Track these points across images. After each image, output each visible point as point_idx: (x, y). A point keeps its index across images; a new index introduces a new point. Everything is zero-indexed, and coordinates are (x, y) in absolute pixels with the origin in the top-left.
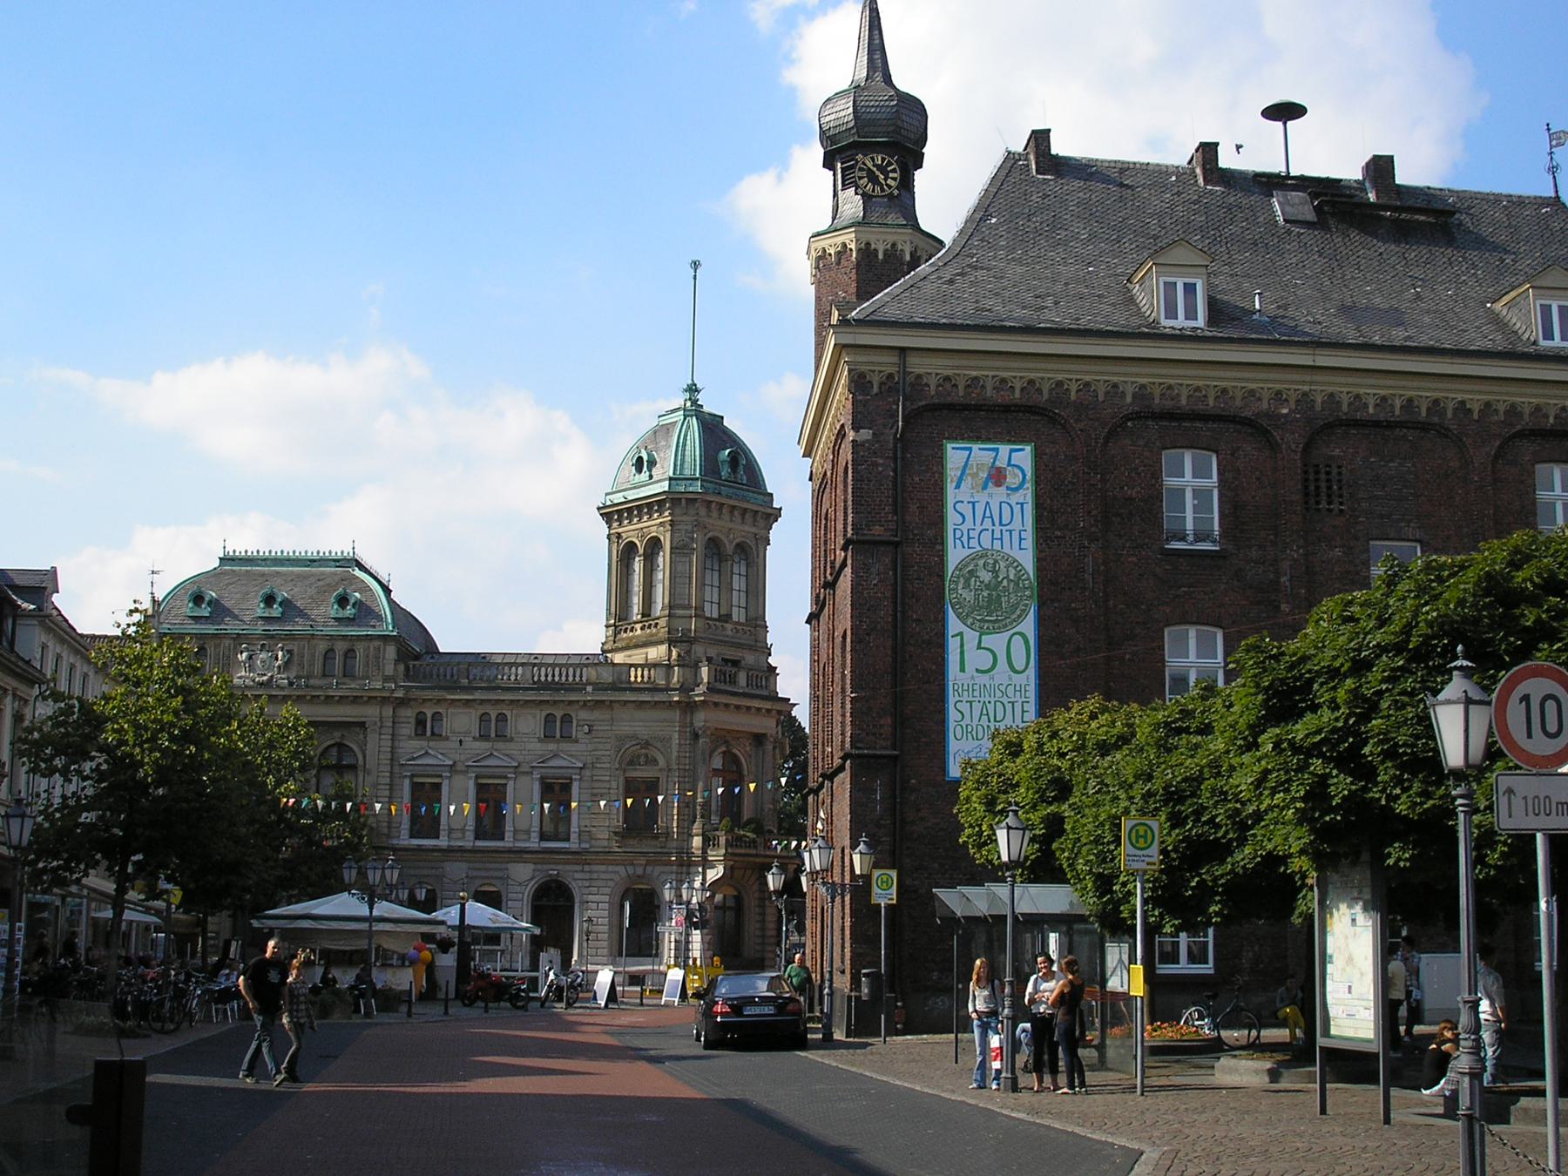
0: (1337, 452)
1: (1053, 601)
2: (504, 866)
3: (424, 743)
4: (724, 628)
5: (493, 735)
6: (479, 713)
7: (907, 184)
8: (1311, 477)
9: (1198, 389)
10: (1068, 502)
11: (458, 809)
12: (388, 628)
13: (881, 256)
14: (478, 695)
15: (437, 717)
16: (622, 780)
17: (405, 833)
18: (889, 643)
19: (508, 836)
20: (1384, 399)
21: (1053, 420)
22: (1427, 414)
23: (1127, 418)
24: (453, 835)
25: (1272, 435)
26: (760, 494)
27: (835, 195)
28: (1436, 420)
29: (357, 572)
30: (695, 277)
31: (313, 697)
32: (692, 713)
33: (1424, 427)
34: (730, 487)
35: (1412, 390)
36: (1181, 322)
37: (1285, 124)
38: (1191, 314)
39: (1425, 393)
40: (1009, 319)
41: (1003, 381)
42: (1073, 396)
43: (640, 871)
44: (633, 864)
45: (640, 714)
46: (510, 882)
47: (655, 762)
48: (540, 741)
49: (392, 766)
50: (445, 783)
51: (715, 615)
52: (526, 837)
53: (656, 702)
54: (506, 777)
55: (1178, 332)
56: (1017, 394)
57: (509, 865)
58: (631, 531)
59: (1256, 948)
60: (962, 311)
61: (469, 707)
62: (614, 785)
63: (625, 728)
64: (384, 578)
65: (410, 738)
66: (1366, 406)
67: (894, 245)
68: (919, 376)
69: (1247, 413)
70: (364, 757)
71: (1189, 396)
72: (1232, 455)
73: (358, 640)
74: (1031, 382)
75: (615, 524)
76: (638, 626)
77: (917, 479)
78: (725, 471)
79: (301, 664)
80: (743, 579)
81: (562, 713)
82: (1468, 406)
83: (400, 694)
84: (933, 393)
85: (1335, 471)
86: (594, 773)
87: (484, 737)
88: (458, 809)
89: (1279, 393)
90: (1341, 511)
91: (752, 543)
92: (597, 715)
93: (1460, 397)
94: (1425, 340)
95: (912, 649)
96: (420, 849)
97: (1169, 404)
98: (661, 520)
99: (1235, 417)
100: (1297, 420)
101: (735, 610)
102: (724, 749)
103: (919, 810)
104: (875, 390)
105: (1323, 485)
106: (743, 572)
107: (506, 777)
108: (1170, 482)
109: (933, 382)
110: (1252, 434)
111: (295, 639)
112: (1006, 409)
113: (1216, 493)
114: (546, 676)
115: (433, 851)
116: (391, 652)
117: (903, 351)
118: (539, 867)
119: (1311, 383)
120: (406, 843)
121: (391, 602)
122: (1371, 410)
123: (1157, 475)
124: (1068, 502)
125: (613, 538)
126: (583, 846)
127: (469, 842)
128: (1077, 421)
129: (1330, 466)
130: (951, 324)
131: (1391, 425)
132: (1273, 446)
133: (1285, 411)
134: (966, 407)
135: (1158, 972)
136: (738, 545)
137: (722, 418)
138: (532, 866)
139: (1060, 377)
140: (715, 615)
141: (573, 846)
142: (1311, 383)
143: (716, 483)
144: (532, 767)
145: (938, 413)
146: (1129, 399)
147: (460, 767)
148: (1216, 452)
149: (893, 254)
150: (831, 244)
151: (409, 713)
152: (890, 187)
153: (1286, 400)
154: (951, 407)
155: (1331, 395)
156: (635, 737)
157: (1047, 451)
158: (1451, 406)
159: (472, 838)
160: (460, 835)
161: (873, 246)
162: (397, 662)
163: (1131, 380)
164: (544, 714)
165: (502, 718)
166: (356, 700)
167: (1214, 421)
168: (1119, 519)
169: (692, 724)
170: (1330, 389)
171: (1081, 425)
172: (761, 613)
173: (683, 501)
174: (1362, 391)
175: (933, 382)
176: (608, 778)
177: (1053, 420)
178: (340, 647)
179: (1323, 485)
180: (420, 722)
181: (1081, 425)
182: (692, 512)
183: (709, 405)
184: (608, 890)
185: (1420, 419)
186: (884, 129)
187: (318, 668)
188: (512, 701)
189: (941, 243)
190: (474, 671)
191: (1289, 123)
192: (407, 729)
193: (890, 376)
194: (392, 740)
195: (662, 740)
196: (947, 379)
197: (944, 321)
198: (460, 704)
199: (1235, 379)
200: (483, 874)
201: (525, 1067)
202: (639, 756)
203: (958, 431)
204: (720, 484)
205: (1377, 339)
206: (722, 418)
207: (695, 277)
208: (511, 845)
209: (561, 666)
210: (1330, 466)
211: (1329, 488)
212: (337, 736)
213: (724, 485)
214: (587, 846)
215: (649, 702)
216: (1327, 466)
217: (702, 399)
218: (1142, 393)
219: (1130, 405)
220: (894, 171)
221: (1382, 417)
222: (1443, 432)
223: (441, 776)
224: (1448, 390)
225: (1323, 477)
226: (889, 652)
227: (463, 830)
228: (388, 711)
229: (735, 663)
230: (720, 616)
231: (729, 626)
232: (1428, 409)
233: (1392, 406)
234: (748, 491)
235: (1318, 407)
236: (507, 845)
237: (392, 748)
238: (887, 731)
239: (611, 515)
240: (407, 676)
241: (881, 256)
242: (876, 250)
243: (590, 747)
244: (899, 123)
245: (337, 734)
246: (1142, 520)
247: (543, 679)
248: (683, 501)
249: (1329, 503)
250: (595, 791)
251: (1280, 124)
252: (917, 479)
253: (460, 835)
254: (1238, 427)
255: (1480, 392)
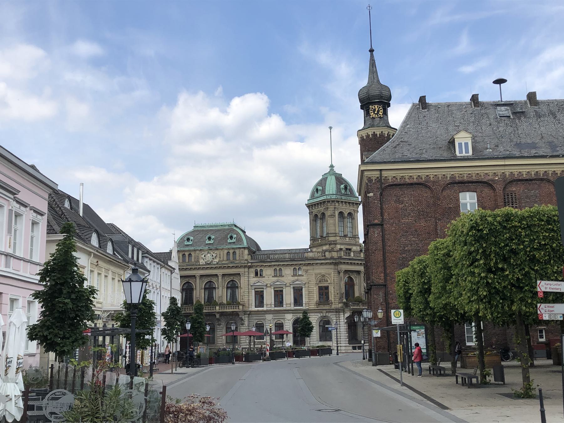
0: (514, 189)
1: (428, 238)
2: (283, 315)
3: (258, 279)
4: (346, 239)
5: (278, 275)
6: (274, 268)
7: (385, 113)
8: (506, 197)
9: (469, 174)
10: (432, 210)
11: (269, 297)
12: (245, 244)
13: (378, 136)
14: (273, 264)
15: (261, 270)
16: (317, 287)
17: (254, 306)
18: (382, 253)
19: (284, 306)
20: (528, 172)
21: (426, 186)
22: (543, 176)
23: (448, 184)
24: (268, 306)
25: (493, 186)
26: (354, 197)
27: (364, 118)
28: (545, 177)
29: (235, 228)
30: (331, 132)
31: (224, 267)
32: (337, 265)
33: (542, 180)
34: (345, 196)
35: (537, 169)
36: (464, 154)
37: (500, 85)
38: (467, 152)
39: (542, 170)
40: (412, 158)
41: (411, 176)
42: (432, 179)
43: (324, 315)
44: (322, 313)
45: (322, 267)
46: (286, 320)
47: (327, 281)
48: (292, 276)
49: (248, 286)
50: (265, 290)
51: (343, 235)
52: (289, 306)
53: (326, 263)
54: (283, 288)
55: (463, 158)
56: (415, 180)
57: (285, 315)
58: (315, 211)
59: (497, 337)
60: (398, 156)
61: (271, 267)
62: (315, 288)
63: (317, 271)
64: (243, 228)
65: (254, 277)
66: (523, 175)
67: (382, 132)
68: (386, 177)
69: (485, 180)
70: (240, 284)
71: (467, 176)
72: (481, 193)
73: (236, 249)
74: (419, 176)
75: (311, 209)
76: (319, 240)
77: (387, 206)
78: (343, 191)
79: (220, 258)
80: (351, 223)
81: (298, 267)
82: (556, 172)
83: (250, 264)
84: (390, 181)
85: (514, 195)
86: (309, 285)
87: (275, 276)
88: (269, 297)
89: (495, 173)
90: (516, 207)
91: (353, 213)
92: (309, 267)
93: (553, 170)
94: (541, 153)
95: (388, 254)
96: (258, 311)
97: (461, 179)
98: (324, 207)
99: (481, 181)
100: (501, 181)
101: (349, 233)
102: (348, 276)
103: (393, 300)
104: (374, 181)
105: (510, 199)
106: (351, 221)
107: (283, 288)
108: (462, 201)
109: (390, 178)
110: (487, 186)
111: (218, 250)
112: (412, 184)
113: (477, 204)
114: (293, 257)
115: (262, 311)
116: (246, 252)
117: (381, 170)
118: (294, 315)
119: (504, 170)
120: (254, 309)
121: (246, 236)
122: (524, 176)
123: (458, 200)
124: (432, 210)
125: (311, 213)
126: (307, 308)
127: (273, 308)
128: (433, 186)
129: (512, 194)
130: (394, 161)
131: (531, 180)
132: (494, 189)
133: (497, 178)
134: (400, 185)
135: (467, 345)
136: (348, 213)
137: (341, 174)
138: (292, 315)
139: (427, 174)
140: (343, 235)
141: (304, 308)
142: (504, 170)
143: (340, 195)
144: (290, 284)
145: (392, 187)
146: (449, 179)
147: (268, 285)
148: (475, 192)
149: (382, 135)
150: (364, 134)
151: (253, 270)
152: (380, 115)
153: (497, 175)
154: (396, 185)
155: (511, 172)
156: (320, 274)
157: (425, 195)
158: (550, 172)
159: (274, 307)
160: (270, 306)
161: (376, 133)
162: (248, 255)
163: (449, 173)
164: (293, 268)
165: (280, 270)
166: (236, 267)
167: (475, 183)
168: (447, 214)
169: (337, 269)
170: (511, 171)
171: (434, 187)
172: (357, 233)
173: (331, 202)
174: (521, 171)
175: (390, 178)
176: (313, 287)
177: (426, 186)
178: (231, 251)
179: (510, 199)
180: (256, 274)
181: (434, 187)
182: (333, 204)
183: (337, 170)
184: (316, 319)
185: (540, 178)
186: (378, 97)
187: (225, 258)
188: (283, 265)
189: (396, 130)
190: (271, 256)
191: (501, 84)
192: (253, 275)
193: (378, 177)
194: (248, 282)
195: (329, 274)
196: (394, 177)
197: (393, 160)
198: (267, 266)
199: (481, 171)
200: (278, 317)
201: (51, 373)
202: (322, 279)
203: (398, 192)
204: (342, 195)
205: (526, 155)
206: (341, 174)
207: (331, 132)
208: (285, 308)
209: (297, 253)
210: (512, 194)
211: (512, 200)
212: (232, 278)
213: (343, 196)
214: (308, 308)
215: (324, 263)
216: (511, 194)
217: (335, 169)
218: (453, 177)
219: (449, 180)
220: (381, 110)
221: (528, 178)
222: (549, 181)
223: (263, 288)
224: (549, 168)
225: (510, 197)
226: (382, 255)
227: (271, 305)
228: (246, 270)
229: (350, 249)
230: (344, 235)
231: (347, 239)
232: (543, 174)
233: (531, 174)
234: (350, 197)
235: (507, 176)
236: (284, 308)
237: (248, 280)
238: (382, 278)
239: (309, 206)
240: (252, 259)
241: (378, 136)
242: (377, 134)
243: (307, 277)
244: (382, 95)
245: (232, 277)
246: (454, 214)
247: (292, 257)
248: (331, 202)
249: (513, 205)
250: (310, 291)
251: (499, 85)
252: (387, 206)
253: (270, 306)
254: (482, 184)
255: (560, 168)
